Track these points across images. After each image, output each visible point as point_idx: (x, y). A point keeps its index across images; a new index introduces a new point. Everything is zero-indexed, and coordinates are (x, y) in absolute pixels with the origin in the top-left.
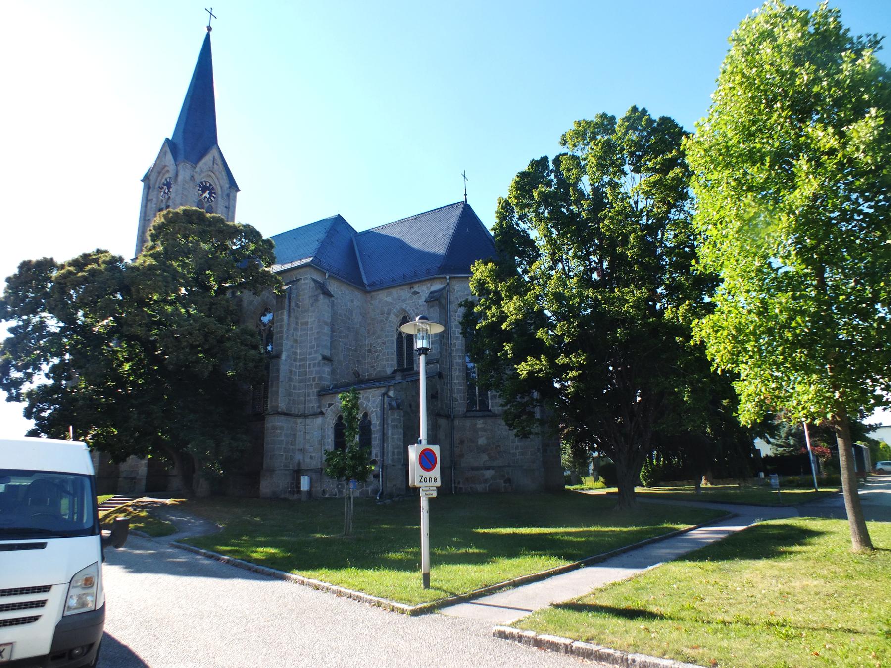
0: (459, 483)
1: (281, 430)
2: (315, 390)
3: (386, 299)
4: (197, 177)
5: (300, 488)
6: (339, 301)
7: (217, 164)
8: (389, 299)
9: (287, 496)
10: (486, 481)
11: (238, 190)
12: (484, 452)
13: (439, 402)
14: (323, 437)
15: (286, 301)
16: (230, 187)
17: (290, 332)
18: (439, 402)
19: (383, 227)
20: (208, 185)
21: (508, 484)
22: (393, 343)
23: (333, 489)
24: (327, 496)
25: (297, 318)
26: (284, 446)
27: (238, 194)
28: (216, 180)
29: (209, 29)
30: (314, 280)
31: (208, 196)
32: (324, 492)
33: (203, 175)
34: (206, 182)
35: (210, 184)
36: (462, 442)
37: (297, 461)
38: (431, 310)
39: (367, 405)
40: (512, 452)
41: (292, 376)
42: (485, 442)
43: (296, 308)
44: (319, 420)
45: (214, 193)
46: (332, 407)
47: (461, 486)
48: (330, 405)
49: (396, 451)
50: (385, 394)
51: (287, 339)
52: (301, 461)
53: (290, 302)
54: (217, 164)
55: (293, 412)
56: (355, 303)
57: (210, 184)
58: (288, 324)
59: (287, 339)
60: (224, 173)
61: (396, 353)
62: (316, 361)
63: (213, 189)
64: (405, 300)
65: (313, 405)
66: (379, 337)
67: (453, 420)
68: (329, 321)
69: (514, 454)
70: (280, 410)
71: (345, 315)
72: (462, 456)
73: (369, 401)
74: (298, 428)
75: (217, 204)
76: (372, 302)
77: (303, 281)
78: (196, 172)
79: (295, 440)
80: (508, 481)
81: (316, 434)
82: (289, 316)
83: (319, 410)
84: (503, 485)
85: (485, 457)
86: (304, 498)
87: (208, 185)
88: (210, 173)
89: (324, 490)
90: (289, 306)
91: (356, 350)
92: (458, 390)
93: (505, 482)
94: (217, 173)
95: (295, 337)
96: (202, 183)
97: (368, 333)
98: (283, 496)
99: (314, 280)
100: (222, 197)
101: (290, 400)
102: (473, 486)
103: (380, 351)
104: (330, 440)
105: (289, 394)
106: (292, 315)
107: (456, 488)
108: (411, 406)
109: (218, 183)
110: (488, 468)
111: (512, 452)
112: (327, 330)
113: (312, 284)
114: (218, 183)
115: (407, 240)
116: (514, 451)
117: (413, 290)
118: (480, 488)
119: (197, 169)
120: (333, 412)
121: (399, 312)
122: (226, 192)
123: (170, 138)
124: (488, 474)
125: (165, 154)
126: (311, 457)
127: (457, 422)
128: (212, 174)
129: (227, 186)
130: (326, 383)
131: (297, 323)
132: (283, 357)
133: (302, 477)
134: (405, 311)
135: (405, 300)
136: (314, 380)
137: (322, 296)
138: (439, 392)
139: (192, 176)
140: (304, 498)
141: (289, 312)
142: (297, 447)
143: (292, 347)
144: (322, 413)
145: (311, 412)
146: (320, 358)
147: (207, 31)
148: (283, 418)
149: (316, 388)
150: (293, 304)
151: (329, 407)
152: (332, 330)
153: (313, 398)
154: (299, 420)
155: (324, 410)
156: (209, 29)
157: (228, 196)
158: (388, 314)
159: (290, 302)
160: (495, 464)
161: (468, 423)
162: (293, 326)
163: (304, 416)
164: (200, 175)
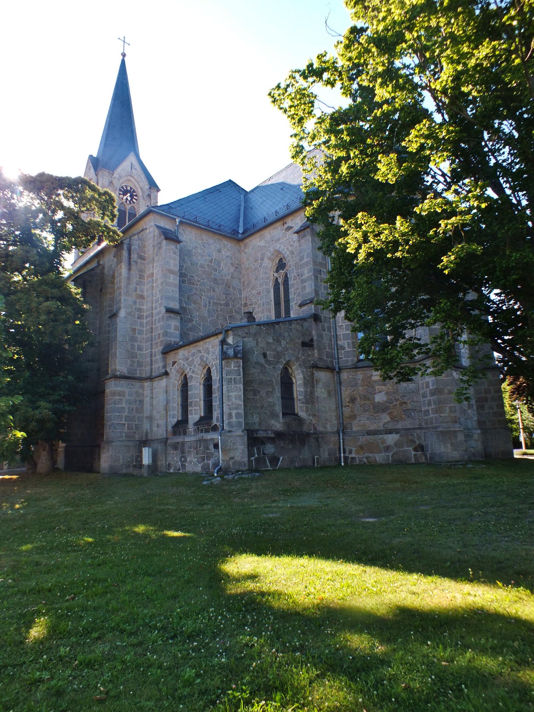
0: (350, 452)
1: (120, 395)
2: (160, 348)
3: (259, 244)
4: (115, 182)
5: (141, 461)
6: (199, 251)
7: (136, 169)
8: (262, 243)
9: (131, 470)
10: (387, 449)
11: (158, 190)
12: (384, 411)
13: (316, 351)
14: (168, 402)
15: (125, 253)
16: (150, 188)
17: (132, 287)
18: (316, 351)
19: (271, 178)
20: (129, 189)
21: (419, 453)
22: (268, 292)
23: (177, 462)
24: (172, 471)
25: (141, 271)
26: (126, 414)
27: (159, 193)
28: (136, 184)
29: (124, 55)
30: (158, 227)
31: (129, 198)
32: (169, 465)
33: (121, 181)
34: (126, 187)
35: (131, 188)
36: (353, 400)
37: (145, 431)
38: (303, 241)
39: (207, 358)
40: (423, 409)
41: (137, 335)
42: (385, 399)
43: (139, 261)
44: (164, 382)
45: (136, 195)
46: (176, 365)
47: (353, 455)
48: (174, 363)
49: (234, 412)
50: (223, 342)
51: (127, 294)
52: (149, 430)
53: (130, 254)
54: (136, 169)
55: (138, 375)
56: (223, 252)
57: (131, 188)
58: (129, 278)
59: (127, 294)
60: (143, 176)
61: (273, 303)
62: (161, 316)
63: (134, 191)
64: (278, 240)
65: (158, 367)
66: (253, 288)
67: (339, 373)
68: (177, 269)
69: (427, 412)
70: (118, 373)
71: (208, 266)
72: (353, 417)
73: (208, 353)
74: (145, 394)
75: (138, 204)
76: (246, 251)
77: (148, 231)
78: (115, 178)
79: (142, 407)
80: (421, 448)
81: (160, 399)
82: (129, 269)
83: (164, 371)
84: (413, 453)
85: (385, 418)
86: (144, 472)
87: (129, 189)
88: (129, 178)
89: (169, 464)
90: (130, 258)
91: (227, 305)
92: (344, 335)
93: (415, 450)
94: (136, 177)
95: (138, 292)
96: (123, 187)
97: (244, 285)
98: (124, 471)
99: (158, 227)
100: (144, 198)
101: (133, 362)
102: (371, 455)
103: (256, 303)
104: (175, 405)
105: (133, 356)
106: (133, 267)
107: (345, 458)
108: (265, 355)
109: (138, 186)
110: (390, 432)
111: (423, 409)
112: (174, 280)
113: (157, 232)
114: (138, 186)
115: (289, 181)
116: (427, 408)
117: (286, 226)
118: (379, 458)
119: (116, 175)
120: (177, 371)
121: (273, 254)
122: (147, 193)
123: (95, 155)
124: (391, 439)
125: (90, 169)
126: (158, 426)
127: (344, 375)
128: (132, 179)
129: (148, 187)
130: (173, 339)
131: (141, 277)
132: (122, 313)
133: (144, 449)
134: (280, 252)
135: (278, 240)
136: (159, 337)
137: (164, 242)
138: (315, 338)
139: (111, 182)
140: (144, 472)
141: (130, 264)
142: (145, 415)
143: (135, 303)
144: (166, 374)
145: (157, 374)
146: (164, 310)
147: (121, 57)
148: (123, 382)
149: (161, 346)
150: (134, 256)
151: (173, 365)
152: (182, 282)
153: (159, 357)
154: (147, 384)
155: (168, 370)
156: (124, 55)
157: (149, 196)
158: (262, 259)
159: (130, 254)
160: (399, 426)
161: (360, 375)
162: (135, 280)
163: (151, 379)
164: (119, 180)
